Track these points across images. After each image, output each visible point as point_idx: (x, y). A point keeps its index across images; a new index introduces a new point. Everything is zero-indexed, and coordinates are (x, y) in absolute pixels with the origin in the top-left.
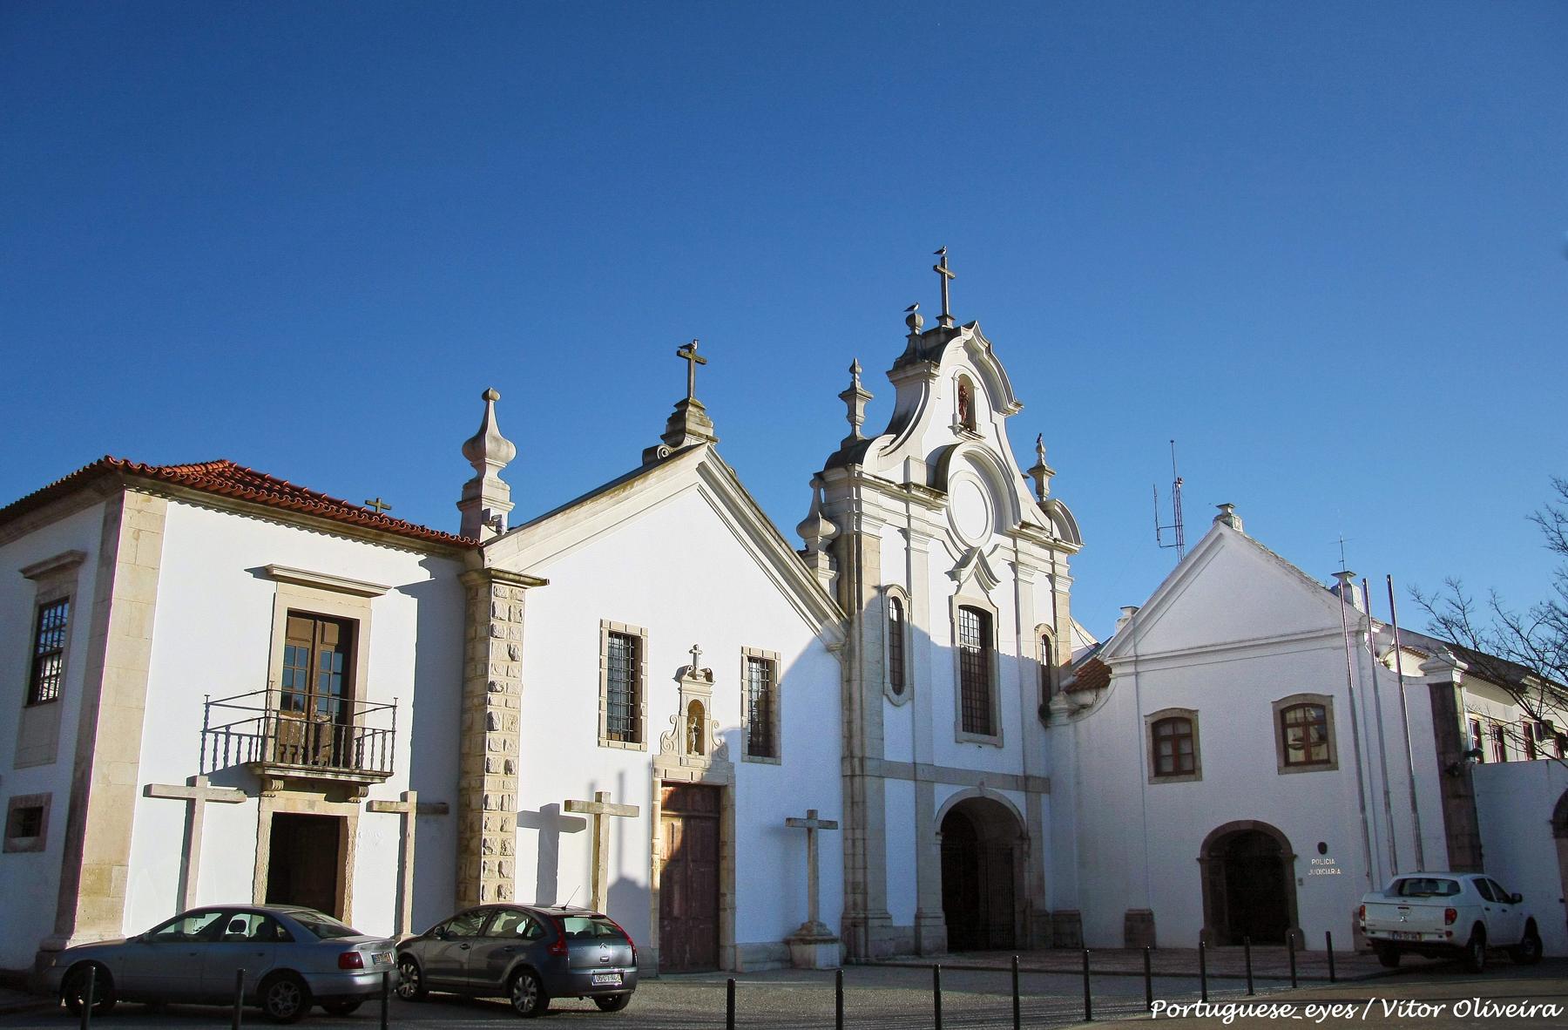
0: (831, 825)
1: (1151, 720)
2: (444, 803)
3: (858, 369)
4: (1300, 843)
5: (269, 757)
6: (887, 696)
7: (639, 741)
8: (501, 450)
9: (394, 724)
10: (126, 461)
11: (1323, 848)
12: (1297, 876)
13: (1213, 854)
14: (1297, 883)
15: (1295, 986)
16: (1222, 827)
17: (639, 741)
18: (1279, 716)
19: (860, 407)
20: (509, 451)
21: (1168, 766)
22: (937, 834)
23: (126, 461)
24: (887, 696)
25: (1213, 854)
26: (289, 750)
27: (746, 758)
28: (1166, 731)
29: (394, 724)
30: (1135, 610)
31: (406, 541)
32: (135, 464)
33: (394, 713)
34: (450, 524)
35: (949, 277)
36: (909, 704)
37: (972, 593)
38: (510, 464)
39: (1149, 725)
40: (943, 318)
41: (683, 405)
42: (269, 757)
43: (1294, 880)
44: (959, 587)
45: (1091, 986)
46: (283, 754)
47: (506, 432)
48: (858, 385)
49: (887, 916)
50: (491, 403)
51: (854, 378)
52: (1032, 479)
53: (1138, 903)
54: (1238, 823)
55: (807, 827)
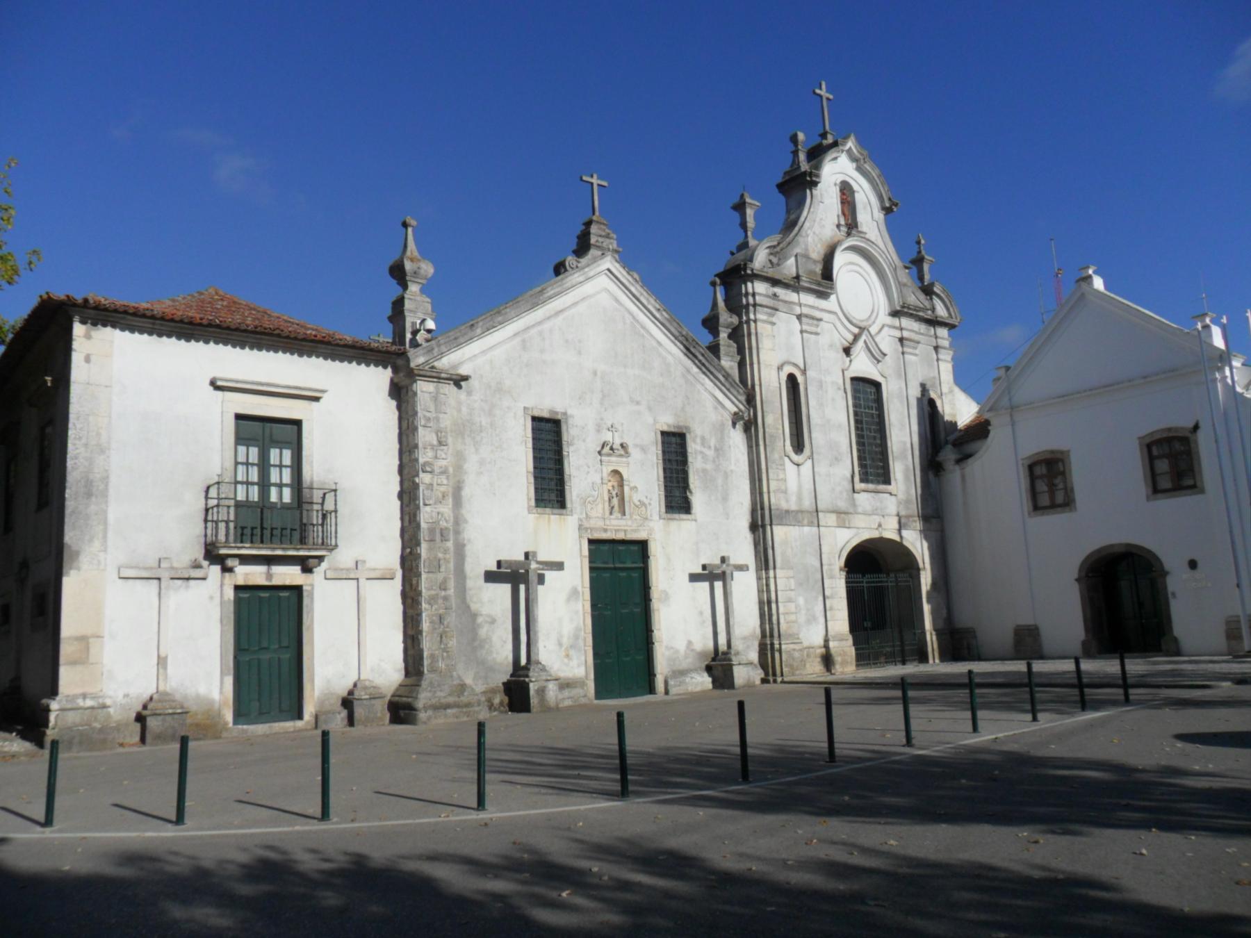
0: (742, 568)
1: (1027, 462)
2: (391, 569)
3: (923, 242)
4: (1172, 559)
5: (222, 537)
6: (788, 457)
7: (537, 506)
8: (421, 268)
9: (336, 504)
10: (47, 293)
11: (1193, 565)
12: (1170, 588)
13: (1090, 575)
14: (1170, 596)
15: (1035, 719)
16: (1099, 551)
17: (537, 506)
18: (1145, 450)
19: (926, 267)
20: (428, 269)
21: (1044, 500)
22: (841, 570)
23: (68, 296)
24: (788, 457)
25: (1090, 575)
26: (248, 532)
27: (664, 515)
28: (1040, 470)
29: (336, 504)
30: (1008, 368)
31: (143, 322)
32: (79, 298)
33: (335, 495)
34: (383, 337)
35: (828, 99)
36: (809, 462)
37: (862, 366)
38: (430, 280)
39: (1026, 466)
40: (824, 135)
41: (588, 224)
42: (222, 537)
43: (1167, 594)
44: (851, 361)
45: (488, 789)
46: (242, 535)
47: (425, 253)
48: (923, 252)
49: (184, 710)
50: (410, 230)
51: (920, 248)
52: (915, 269)
53: (1026, 620)
54: (1112, 546)
55: (713, 575)
